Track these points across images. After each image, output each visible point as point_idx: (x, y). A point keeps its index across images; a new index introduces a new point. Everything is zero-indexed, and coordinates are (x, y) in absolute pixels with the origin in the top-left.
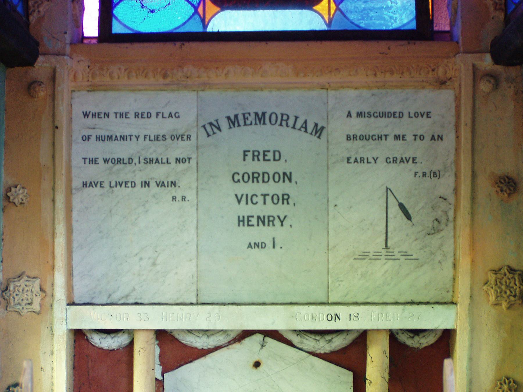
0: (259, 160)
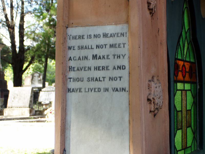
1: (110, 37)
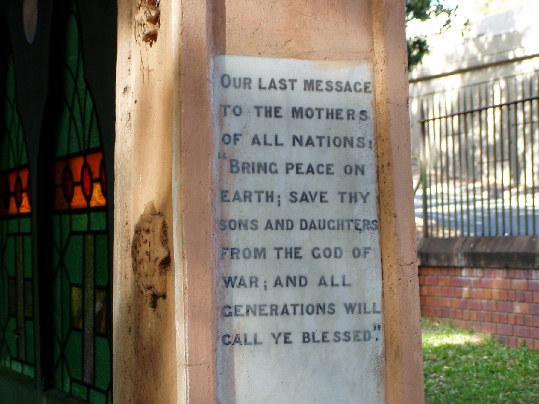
0: (277, 314)
1: (234, 199)
